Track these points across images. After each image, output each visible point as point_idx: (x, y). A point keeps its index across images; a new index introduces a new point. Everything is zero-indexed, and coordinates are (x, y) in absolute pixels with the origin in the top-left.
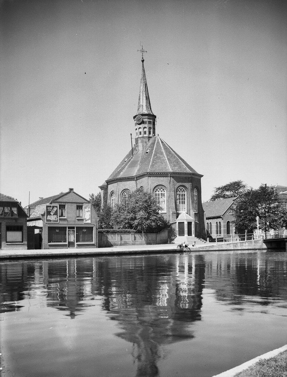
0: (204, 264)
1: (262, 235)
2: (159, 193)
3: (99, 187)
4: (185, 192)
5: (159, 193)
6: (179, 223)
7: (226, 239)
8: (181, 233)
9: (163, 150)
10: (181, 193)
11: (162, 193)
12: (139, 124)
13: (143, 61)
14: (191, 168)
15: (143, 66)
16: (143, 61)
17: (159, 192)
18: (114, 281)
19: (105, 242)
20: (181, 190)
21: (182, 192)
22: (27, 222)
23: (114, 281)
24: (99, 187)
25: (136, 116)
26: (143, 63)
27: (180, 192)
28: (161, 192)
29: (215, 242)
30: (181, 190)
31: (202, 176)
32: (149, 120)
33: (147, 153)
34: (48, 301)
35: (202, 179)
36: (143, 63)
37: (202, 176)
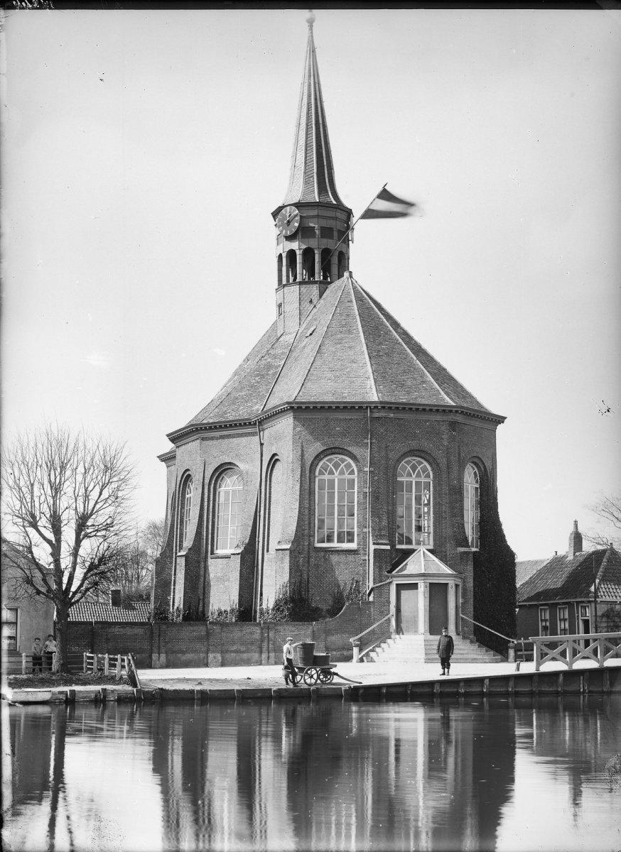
0: (429, 778)
2: (331, 477)
3: (158, 457)
5: (331, 477)
6: (397, 585)
11: (342, 477)
18: (582, 701)
19: (357, 643)
20: (414, 468)
22: (402, 591)
23: (582, 701)
24: (158, 457)
25: (280, 209)
26: (311, 27)
28: (340, 474)
30: (414, 468)
31: (501, 420)
32: (325, 223)
34: (393, 743)
35: (500, 429)
36: (311, 27)
37: (501, 420)
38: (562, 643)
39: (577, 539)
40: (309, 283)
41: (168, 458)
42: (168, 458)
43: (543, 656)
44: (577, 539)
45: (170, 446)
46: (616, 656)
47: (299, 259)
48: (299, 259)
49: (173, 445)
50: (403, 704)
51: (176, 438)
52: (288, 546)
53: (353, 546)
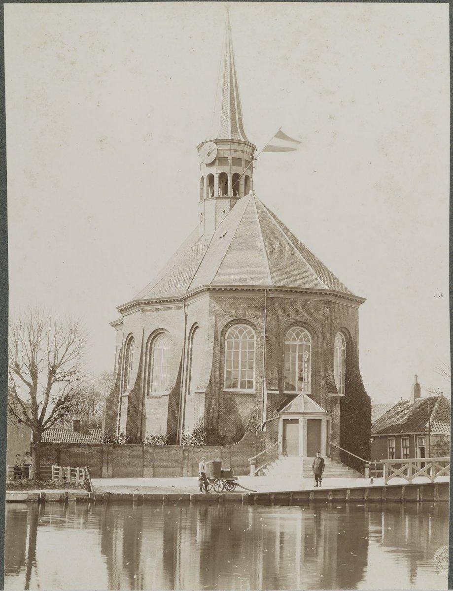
31: (361, 301)
37: (361, 301)
38: (404, 464)
41: (117, 325)
43: (390, 473)
45: (119, 316)
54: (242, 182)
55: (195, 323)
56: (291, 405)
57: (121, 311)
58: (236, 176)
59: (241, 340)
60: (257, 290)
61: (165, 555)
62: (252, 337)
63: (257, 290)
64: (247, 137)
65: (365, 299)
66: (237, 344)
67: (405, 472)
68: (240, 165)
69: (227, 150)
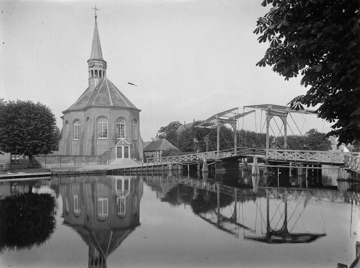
1: (357, 170)
4: (124, 123)
6: (117, 147)
7: (53, 170)
8: (119, 156)
9: (111, 101)
10: (121, 123)
12: (91, 67)
13: (96, 17)
14: (138, 205)
15: (96, 24)
16: (96, 17)
17: (101, 121)
21: (122, 122)
22: (32, 192)
26: (96, 18)
27: (120, 122)
29: (321, 169)
31: (140, 111)
33: (96, 90)
36: (96, 18)
37: (140, 111)
38: (196, 155)
39: (194, 120)
40: (97, 78)
41: (62, 118)
42: (62, 118)
43: (149, 162)
44: (194, 120)
45: (63, 115)
46: (242, 160)
47: (94, 72)
48: (94, 72)
49: (63, 115)
50: (296, 234)
51: (64, 113)
52: (91, 138)
53: (107, 138)
54: (102, 73)
55: (88, 117)
56: (314, 153)
57: (63, 113)
58: (100, 71)
59: (103, 122)
60: (308, 166)
61: (99, 171)
62: (106, 122)
63: (308, 166)
64: (103, 56)
65: (141, 110)
66: (102, 123)
67: (166, 161)
68: (101, 68)
69: (97, 63)
